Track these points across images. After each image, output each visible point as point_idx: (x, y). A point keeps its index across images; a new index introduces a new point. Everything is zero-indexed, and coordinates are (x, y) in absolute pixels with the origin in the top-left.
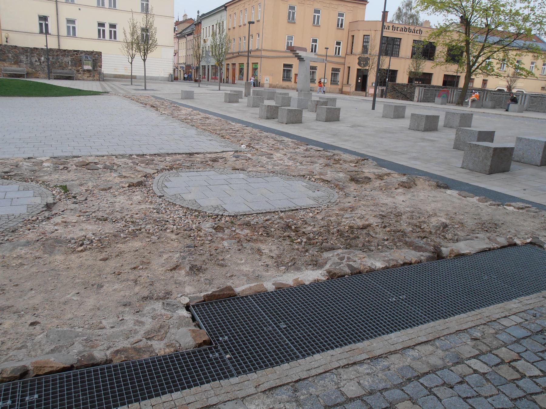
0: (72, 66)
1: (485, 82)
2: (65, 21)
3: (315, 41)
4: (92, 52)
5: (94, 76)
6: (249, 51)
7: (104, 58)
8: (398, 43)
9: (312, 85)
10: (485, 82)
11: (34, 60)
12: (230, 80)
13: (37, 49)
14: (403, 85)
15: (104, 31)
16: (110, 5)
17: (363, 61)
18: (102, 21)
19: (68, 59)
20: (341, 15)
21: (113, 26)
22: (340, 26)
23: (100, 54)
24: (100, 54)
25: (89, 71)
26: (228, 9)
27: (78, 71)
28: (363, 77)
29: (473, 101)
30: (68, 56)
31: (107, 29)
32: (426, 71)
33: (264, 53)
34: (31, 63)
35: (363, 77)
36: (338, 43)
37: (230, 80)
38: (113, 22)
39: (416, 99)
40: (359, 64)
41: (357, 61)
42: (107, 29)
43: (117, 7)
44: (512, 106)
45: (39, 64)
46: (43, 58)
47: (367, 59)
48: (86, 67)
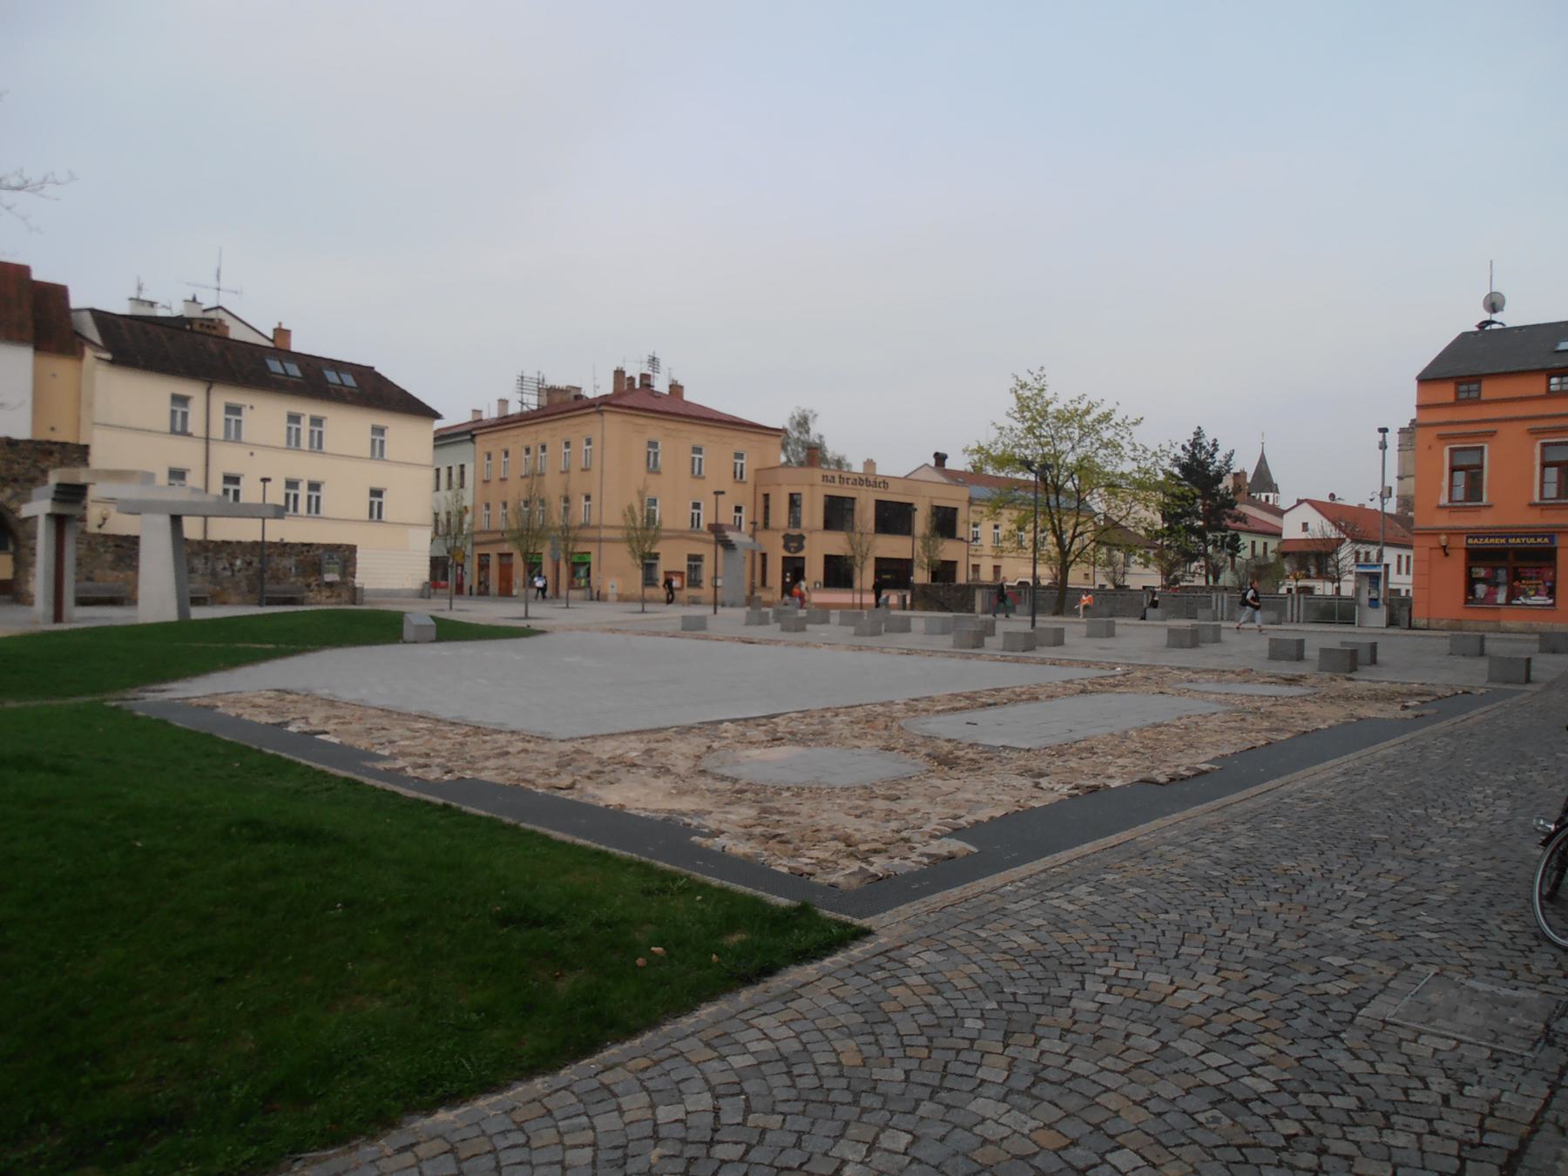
0: (297, 575)
1: (997, 569)
2: (221, 479)
3: (696, 506)
4: (339, 546)
5: (339, 595)
6: (566, 528)
7: (362, 559)
8: (847, 506)
9: (650, 591)
10: (997, 569)
11: (220, 566)
12: (494, 585)
13: (228, 543)
14: (924, 586)
15: (296, 497)
16: (311, 445)
17: (794, 541)
18: (294, 476)
19: (289, 562)
20: (739, 456)
21: (314, 486)
22: (738, 476)
23: (352, 549)
24: (352, 549)
25: (330, 585)
26: (478, 439)
27: (309, 586)
28: (794, 569)
29: (1086, 607)
30: (290, 555)
31: (303, 491)
32: (944, 558)
33: (605, 534)
34: (214, 574)
35: (794, 569)
36: (738, 509)
37: (494, 585)
38: (316, 478)
39: (978, 608)
40: (786, 547)
41: (782, 542)
42: (303, 491)
43: (244, 437)
44: (1150, 612)
45: (229, 573)
46: (238, 562)
47: (801, 538)
48: (329, 577)
